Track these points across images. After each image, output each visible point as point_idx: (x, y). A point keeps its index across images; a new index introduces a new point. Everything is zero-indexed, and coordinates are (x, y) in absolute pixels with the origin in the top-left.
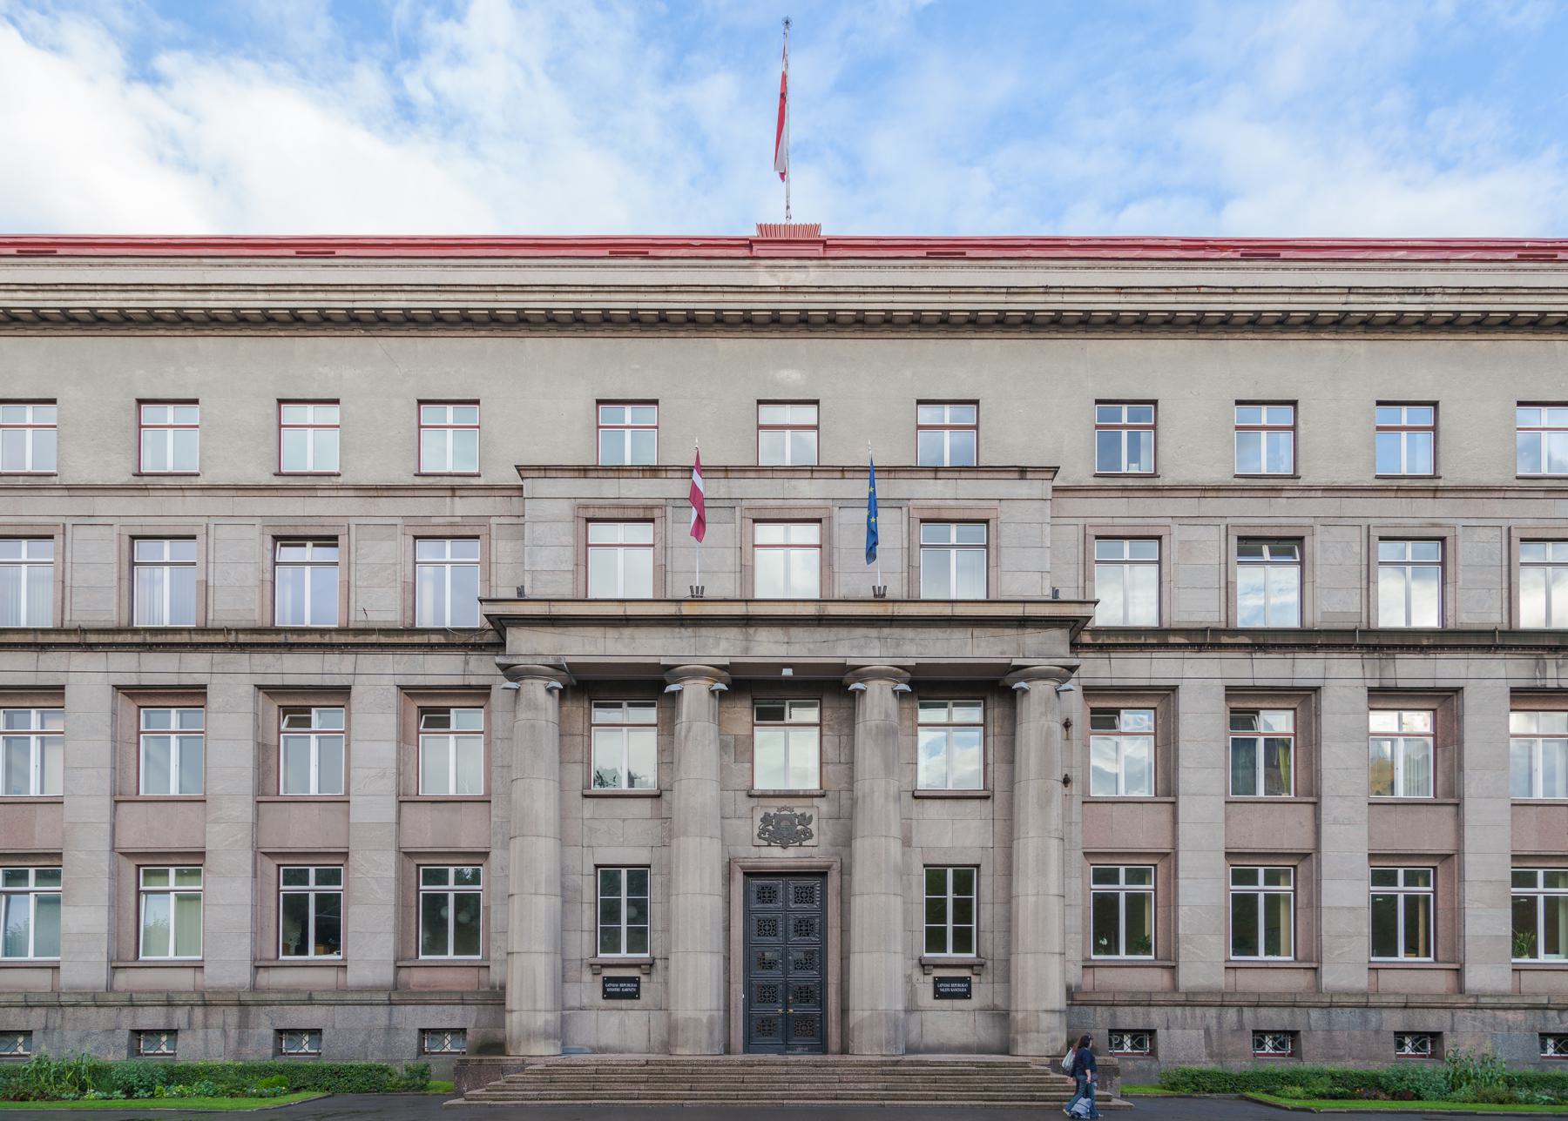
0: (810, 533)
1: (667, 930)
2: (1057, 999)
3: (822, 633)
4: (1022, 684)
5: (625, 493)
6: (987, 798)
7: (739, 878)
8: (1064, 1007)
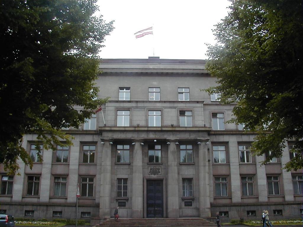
0: (159, 113)
1: (132, 192)
2: (208, 206)
3: (161, 133)
4: (199, 143)
5: (125, 106)
6: (194, 164)
7: (145, 181)
8: (210, 207)
